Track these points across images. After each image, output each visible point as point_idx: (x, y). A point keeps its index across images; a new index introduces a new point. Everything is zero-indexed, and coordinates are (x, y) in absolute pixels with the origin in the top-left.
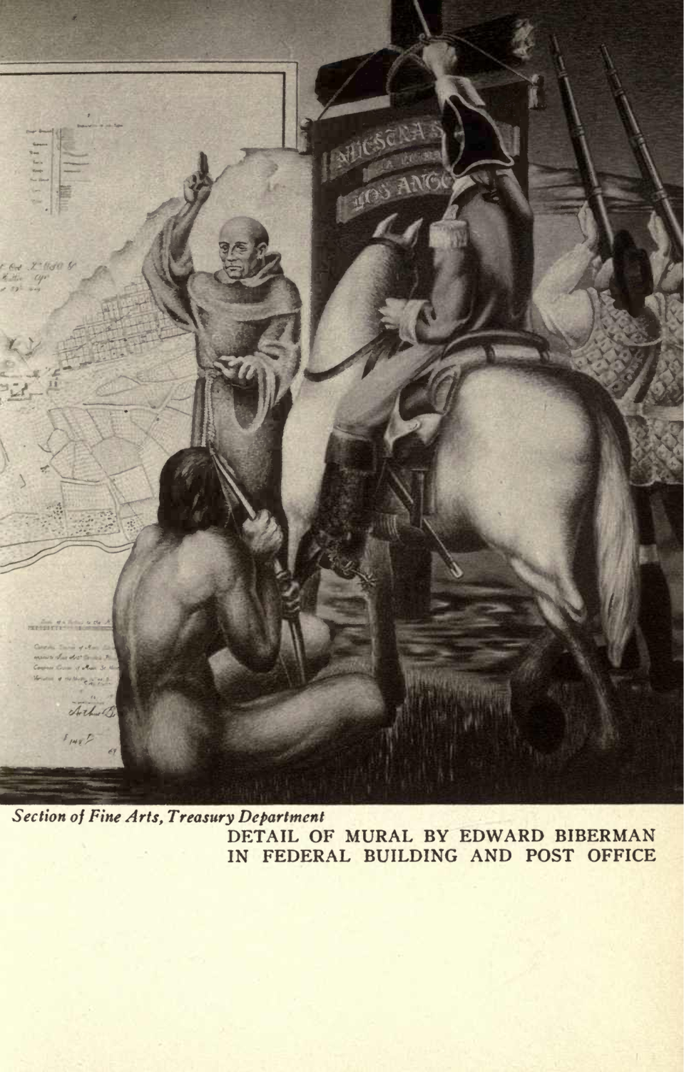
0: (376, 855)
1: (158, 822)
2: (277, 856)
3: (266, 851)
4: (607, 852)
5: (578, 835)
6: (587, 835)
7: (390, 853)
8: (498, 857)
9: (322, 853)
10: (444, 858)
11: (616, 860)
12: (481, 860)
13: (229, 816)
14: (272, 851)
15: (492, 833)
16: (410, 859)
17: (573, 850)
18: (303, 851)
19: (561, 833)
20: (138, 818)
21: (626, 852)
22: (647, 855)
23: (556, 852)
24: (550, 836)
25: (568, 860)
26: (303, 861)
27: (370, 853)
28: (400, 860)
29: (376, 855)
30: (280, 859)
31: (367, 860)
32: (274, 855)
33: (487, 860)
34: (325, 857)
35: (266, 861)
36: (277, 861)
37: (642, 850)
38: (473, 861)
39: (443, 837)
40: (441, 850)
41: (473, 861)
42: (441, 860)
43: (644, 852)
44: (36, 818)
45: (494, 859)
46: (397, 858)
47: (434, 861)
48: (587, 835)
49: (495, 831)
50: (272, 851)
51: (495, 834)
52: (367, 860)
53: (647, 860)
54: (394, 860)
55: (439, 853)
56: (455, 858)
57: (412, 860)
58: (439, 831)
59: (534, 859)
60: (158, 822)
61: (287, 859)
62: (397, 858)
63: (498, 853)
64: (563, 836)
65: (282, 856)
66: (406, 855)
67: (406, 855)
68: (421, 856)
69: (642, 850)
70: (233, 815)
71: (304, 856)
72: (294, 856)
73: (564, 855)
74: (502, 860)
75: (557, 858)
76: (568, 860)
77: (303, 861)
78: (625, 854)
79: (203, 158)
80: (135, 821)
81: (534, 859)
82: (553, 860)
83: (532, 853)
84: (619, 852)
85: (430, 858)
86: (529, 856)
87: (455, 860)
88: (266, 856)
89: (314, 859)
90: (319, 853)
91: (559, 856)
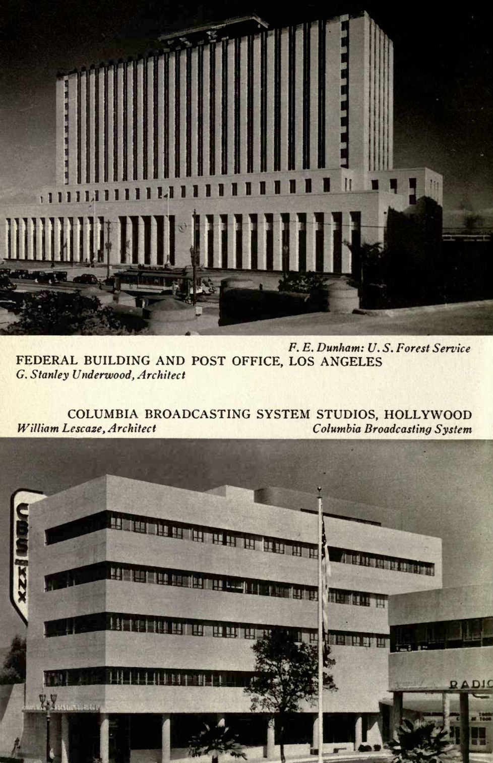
0: (92, 360)
1: (131, 378)
2: (26, 360)
3: (18, 357)
4: (246, 359)
5: (118, 414)
6: (153, 414)
7: (103, 358)
8: (175, 362)
9: (58, 358)
10: (140, 362)
11: (252, 364)
12: (327, 365)
13: (65, 374)
14: (257, 357)
15: (435, 413)
16: (117, 363)
17: (225, 357)
18: (45, 357)
19: (120, 412)
20: (146, 376)
21: (259, 359)
22: (274, 361)
23: (213, 359)
24: (141, 414)
25: (221, 364)
26: (45, 363)
27: (88, 358)
28: (110, 364)
29: (92, 360)
30: (28, 362)
31: (86, 364)
32: (24, 359)
33: (168, 364)
34: (60, 361)
35: (18, 363)
36: (26, 363)
37: (270, 358)
38: (322, 365)
39: (269, 415)
40: (338, 358)
41: (322, 365)
42: (138, 363)
43: (272, 358)
44: (179, 376)
45: (173, 363)
46: (107, 362)
47: (133, 364)
48: (153, 414)
49: (437, 411)
50: (23, 357)
51: (437, 413)
52: (86, 364)
53: (274, 365)
54: (105, 364)
55: (137, 359)
56: (148, 362)
57: (118, 364)
58: (266, 411)
59: (198, 363)
60: (131, 378)
61: (33, 362)
62: (107, 362)
63: (175, 359)
64: (370, 428)
65: (355, 361)
66: (364, 361)
67: (364, 361)
68: (124, 360)
69: (270, 358)
70: (68, 374)
71: (45, 360)
72: (38, 360)
73: (218, 361)
74: (178, 364)
75: (213, 363)
76: (221, 364)
77: (45, 363)
78: (258, 360)
79: (131, 371)
80: (144, 378)
81: (198, 363)
82: (211, 364)
83: (196, 359)
84: (254, 359)
85: (131, 362)
86: (194, 361)
87: (148, 364)
88: (18, 360)
89: (52, 362)
90: (56, 358)
91: (215, 362)
